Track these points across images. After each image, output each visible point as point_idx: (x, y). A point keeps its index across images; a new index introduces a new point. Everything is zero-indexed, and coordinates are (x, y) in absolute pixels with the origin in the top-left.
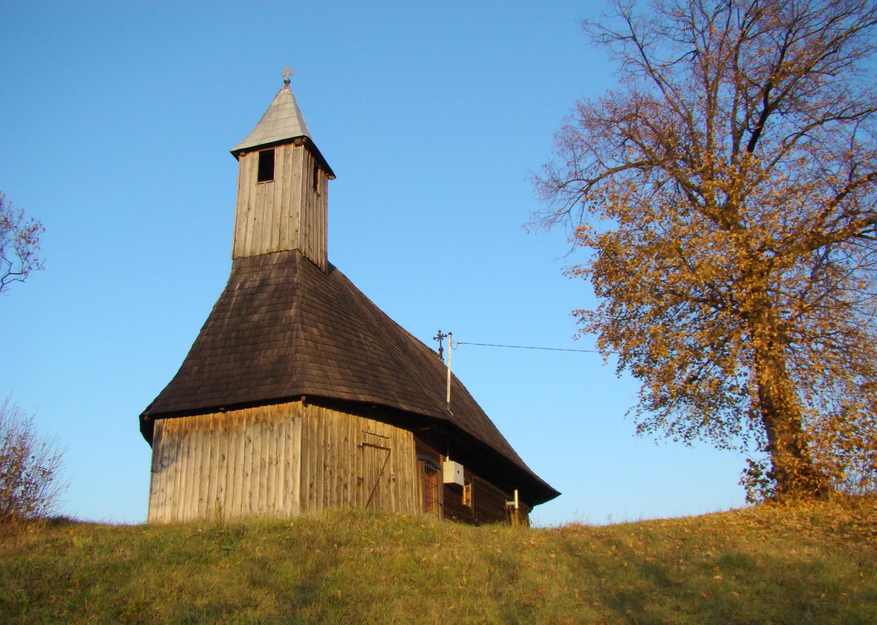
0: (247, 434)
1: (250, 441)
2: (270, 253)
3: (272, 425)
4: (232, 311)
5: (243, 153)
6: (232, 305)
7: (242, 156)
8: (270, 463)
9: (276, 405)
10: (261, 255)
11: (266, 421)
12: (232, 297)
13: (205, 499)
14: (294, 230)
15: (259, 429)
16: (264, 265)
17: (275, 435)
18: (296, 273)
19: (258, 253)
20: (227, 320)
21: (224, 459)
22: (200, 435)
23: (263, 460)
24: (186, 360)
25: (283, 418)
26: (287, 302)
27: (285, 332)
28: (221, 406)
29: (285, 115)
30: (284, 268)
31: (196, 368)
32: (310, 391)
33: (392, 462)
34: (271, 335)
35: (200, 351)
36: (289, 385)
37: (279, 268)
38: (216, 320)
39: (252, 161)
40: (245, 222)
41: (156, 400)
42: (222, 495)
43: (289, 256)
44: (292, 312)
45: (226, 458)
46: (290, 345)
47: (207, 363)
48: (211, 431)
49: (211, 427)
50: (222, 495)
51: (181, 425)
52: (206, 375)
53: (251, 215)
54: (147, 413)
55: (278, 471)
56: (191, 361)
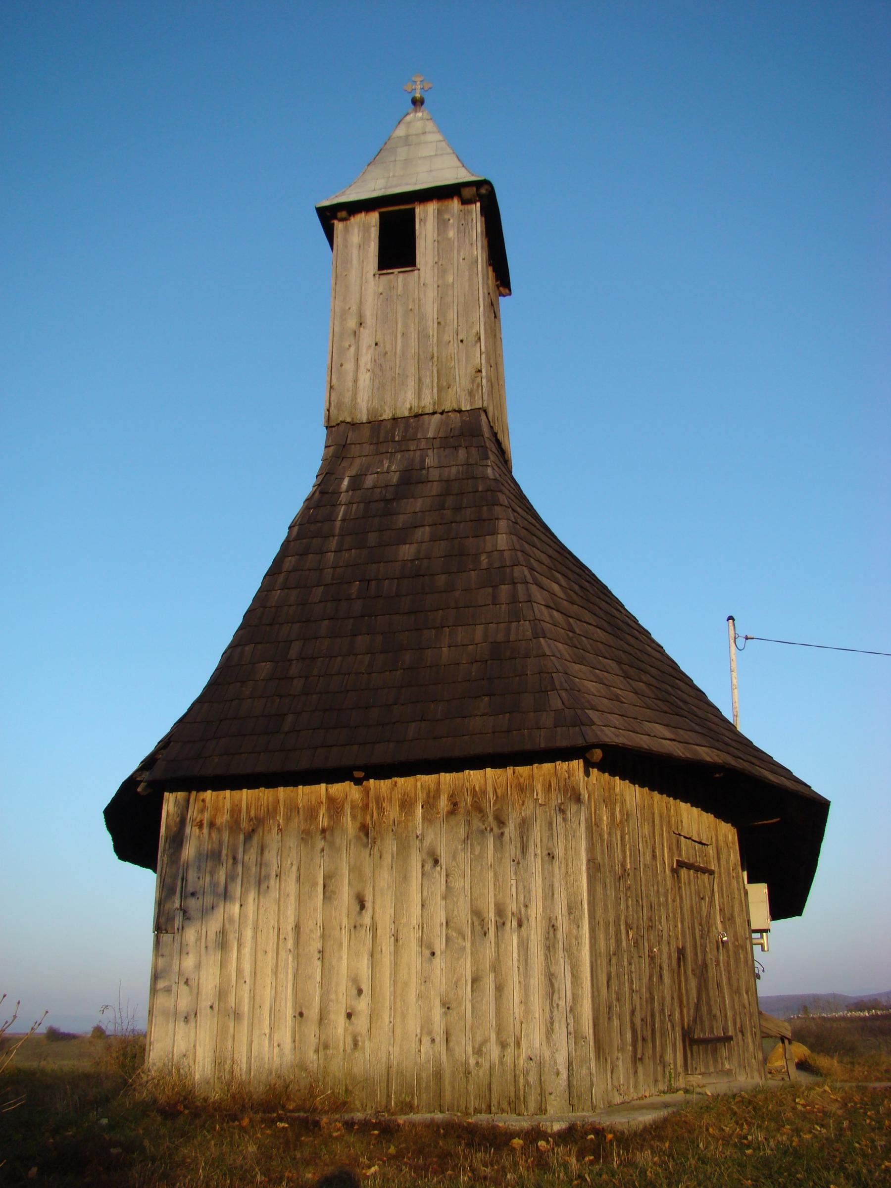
0: (427, 842)
1: (436, 862)
2: (417, 416)
3: (501, 822)
4: (341, 535)
5: (343, 214)
6: (338, 524)
7: (342, 220)
8: (501, 925)
9: (510, 770)
10: (394, 419)
11: (480, 810)
12: (335, 505)
13: (313, 1013)
14: (471, 370)
15: (462, 832)
16: (404, 439)
17: (512, 849)
18: (487, 458)
19: (387, 415)
20: (331, 556)
21: (362, 907)
22: (292, 842)
23: (477, 913)
24: (232, 647)
25: (530, 805)
26: (480, 520)
27: (495, 587)
28: (359, 769)
29: (426, 151)
30: (456, 448)
31: (265, 668)
32: (611, 736)
33: (717, 903)
34: (457, 594)
35: (271, 625)
36: (547, 719)
37: (443, 447)
38: (303, 554)
39: (366, 229)
40: (352, 349)
41: (165, 744)
42: (362, 1005)
43: (463, 422)
44: (502, 540)
45: (369, 905)
46: (515, 616)
47: (293, 653)
48: (324, 831)
49: (323, 820)
50: (362, 1005)
51: (235, 811)
52: (298, 685)
53: (367, 337)
54: (146, 775)
55: (524, 946)
56: (248, 649)
